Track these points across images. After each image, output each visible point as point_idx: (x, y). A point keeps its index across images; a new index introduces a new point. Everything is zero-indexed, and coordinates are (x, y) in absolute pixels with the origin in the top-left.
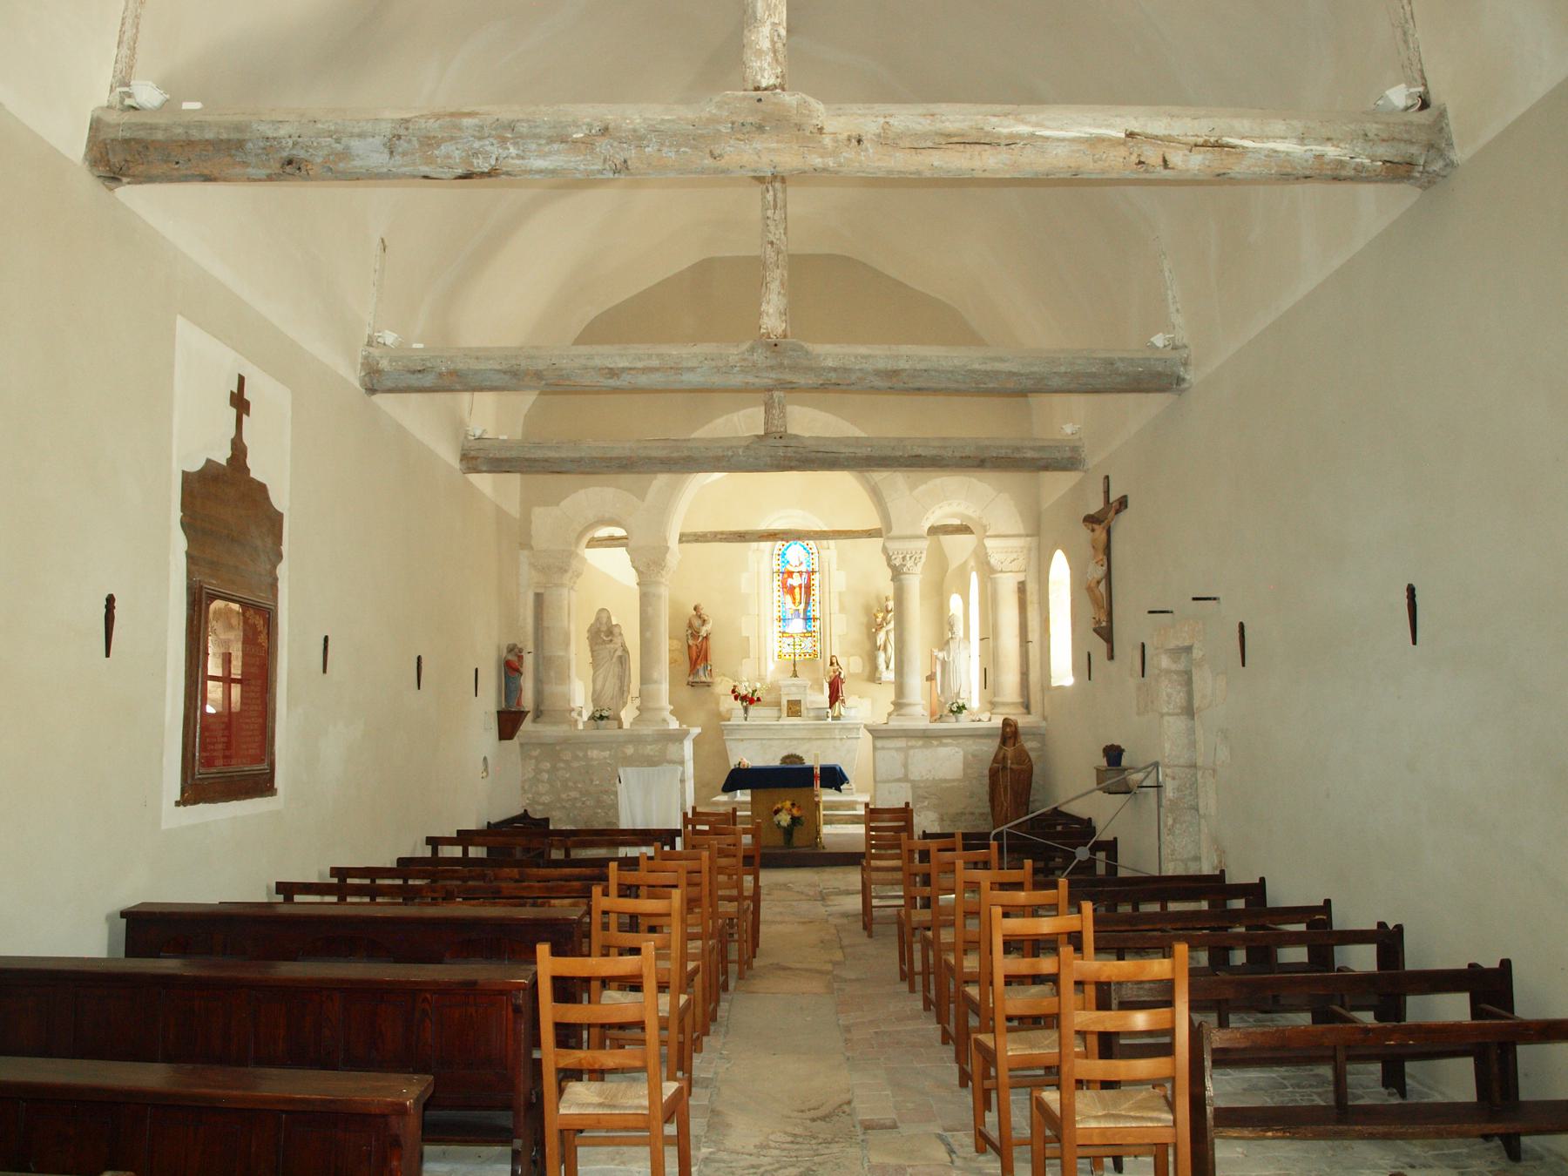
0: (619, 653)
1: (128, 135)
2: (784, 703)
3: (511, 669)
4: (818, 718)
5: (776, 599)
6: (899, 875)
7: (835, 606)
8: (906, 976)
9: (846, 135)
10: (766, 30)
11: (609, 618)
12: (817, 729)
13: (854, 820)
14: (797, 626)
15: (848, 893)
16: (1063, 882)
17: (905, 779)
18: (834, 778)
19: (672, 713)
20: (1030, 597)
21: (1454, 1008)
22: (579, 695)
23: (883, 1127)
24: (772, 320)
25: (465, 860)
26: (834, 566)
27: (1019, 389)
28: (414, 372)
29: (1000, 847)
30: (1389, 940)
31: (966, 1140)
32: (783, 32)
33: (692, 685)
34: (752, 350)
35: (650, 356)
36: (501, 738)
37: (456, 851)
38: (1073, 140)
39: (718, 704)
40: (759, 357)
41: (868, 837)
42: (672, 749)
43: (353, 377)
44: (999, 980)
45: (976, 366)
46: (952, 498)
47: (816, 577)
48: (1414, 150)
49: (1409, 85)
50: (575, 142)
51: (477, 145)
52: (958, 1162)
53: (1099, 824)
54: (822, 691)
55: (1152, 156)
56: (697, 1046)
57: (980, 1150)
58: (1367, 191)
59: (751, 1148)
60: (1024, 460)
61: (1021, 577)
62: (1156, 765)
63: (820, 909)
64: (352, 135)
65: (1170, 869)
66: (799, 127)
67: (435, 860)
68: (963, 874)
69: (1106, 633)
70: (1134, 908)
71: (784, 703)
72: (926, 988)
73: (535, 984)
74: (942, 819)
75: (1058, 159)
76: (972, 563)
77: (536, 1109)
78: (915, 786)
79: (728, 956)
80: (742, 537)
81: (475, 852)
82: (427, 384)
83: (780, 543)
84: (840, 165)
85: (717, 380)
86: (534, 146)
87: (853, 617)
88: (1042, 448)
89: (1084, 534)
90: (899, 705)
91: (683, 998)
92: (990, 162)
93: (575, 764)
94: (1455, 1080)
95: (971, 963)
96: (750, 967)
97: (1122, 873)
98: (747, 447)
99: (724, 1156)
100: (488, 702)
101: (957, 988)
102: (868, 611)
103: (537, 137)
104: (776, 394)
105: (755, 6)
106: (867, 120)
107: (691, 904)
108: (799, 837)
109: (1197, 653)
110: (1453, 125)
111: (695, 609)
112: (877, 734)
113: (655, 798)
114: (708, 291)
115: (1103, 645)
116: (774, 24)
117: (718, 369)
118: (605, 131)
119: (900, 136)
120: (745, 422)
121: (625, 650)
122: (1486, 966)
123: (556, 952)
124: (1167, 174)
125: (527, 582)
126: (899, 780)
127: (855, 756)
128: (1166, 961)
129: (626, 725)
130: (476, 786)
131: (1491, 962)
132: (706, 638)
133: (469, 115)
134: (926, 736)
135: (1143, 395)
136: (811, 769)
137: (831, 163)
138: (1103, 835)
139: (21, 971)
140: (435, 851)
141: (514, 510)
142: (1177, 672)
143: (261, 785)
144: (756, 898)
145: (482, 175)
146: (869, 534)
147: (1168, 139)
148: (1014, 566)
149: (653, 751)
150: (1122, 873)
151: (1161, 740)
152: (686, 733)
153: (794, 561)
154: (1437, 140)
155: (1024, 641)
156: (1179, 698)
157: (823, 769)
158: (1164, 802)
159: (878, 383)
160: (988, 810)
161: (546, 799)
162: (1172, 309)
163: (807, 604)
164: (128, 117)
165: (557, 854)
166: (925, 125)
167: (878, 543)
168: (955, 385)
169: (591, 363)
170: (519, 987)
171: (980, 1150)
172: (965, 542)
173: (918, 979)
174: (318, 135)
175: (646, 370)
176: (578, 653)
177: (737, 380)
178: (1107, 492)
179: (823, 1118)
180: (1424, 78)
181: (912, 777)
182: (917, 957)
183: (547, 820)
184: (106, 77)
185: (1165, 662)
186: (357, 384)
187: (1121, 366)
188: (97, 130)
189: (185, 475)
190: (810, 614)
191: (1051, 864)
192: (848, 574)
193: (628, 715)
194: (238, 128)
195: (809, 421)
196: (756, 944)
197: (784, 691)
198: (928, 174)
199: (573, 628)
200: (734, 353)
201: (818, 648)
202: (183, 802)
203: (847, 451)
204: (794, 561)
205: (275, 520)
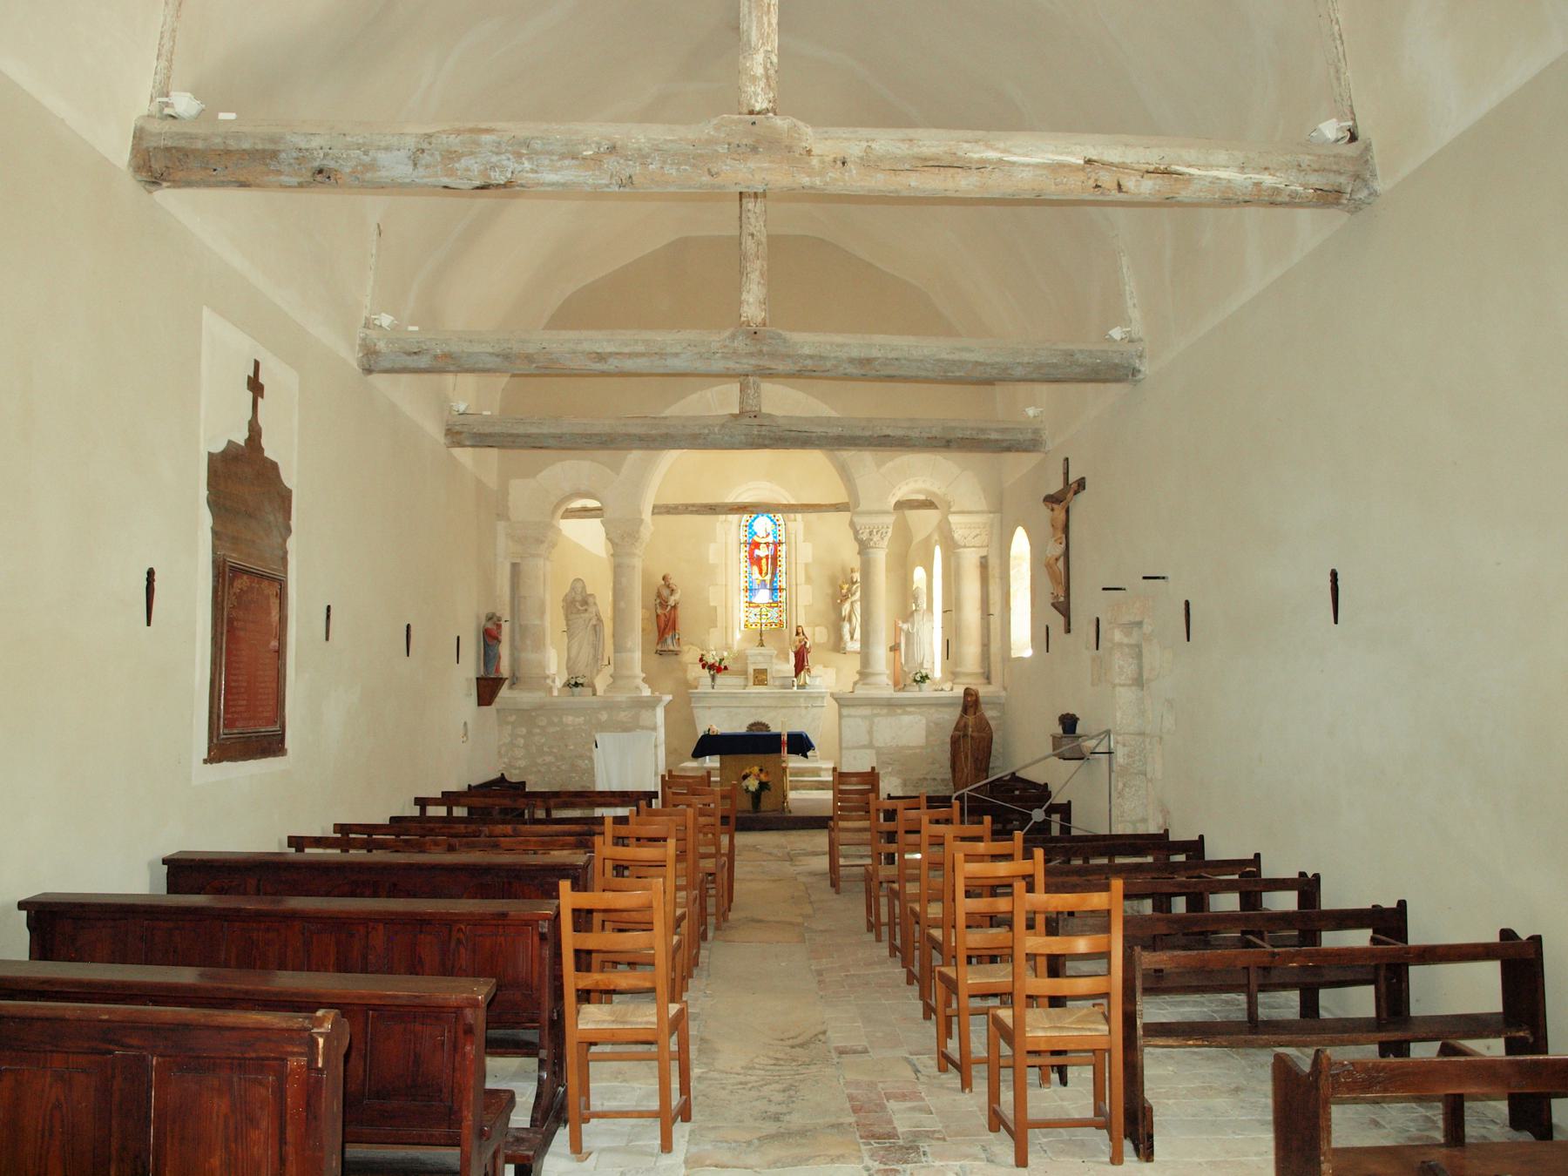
0: (594, 622)
1: (169, 143)
2: (751, 671)
3: (490, 637)
4: (783, 687)
5: (743, 569)
6: (867, 836)
7: (802, 578)
8: (873, 926)
9: (831, 158)
10: (760, 57)
11: (584, 587)
13: (821, 786)
14: (763, 596)
15: (815, 854)
16: (1019, 835)
17: (870, 746)
18: (800, 744)
19: (644, 680)
20: (993, 572)
21: (1360, 938)
22: (554, 663)
23: (855, 1052)
24: (753, 305)
25: (449, 819)
26: (801, 537)
27: (987, 379)
28: (409, 354)
29: (962, 809)
30: (1308, 887)
31: (929, 1062)
32: (775, 60)
33: (660, 653)
34: (733, 337)
35: (636, 341)
36: (480, 704)
37: (441, 811)
38: (1037, 166)
39: (685, 671)
40: (740, 344)
41: (835, 800)
42: (645, 715)
43: (352, 358)
44: (961, 921)
45: (944, 356)
46: (918, 474)
47: (783, 548)
48: (1342, 179)
49: (1341, 118)
50: (584, 158)
51: (494, 159)
52: (922, 1079)
53: (1053, 788)
55: (1107, 179)
56: (684, 988)
57: (942, 1069)
58: (1304, 215)
59: (738, 1069)
60: (988, 441)
61: (983, 552)
62: (1108, 733)
63: (788, 868)
64: (379, 149)
65: (1119, 829)
66: (790, 149)
67: (423, 818)
68: (929, 829)
69: (1064, 608)
70: (1077, 855)
71: (751, 671)
72: (892, 936)
73: (558, 915)
74: (905, 784)
75: (1024, 182)
76: (936, 537)
77: (557, 1028)
79: (711, 906)
80: (713, 509)
81: (460, 812)
82: (422, 366)
83: (746, 517)
84: (826, 184)
85: (700, 366)
86: (547, 162)
87: (832, 591)
88: (1004, 431)
89: (1044, 512)
90: (864, 674)
91: (676, 938)
92: (965, 183)
93: (551, 730)
94: (1360, 1001)
95: (935, 910)
96: (726, 919)
97: (1074, 832)
98: (723, 426)
99: (715, 1075)
100: (469, 668)
101: (922, 932)
102: (833, 581)
103: (551, 153)
104: (751, 379)
105: (749, 35)
106: (852, 143)
107: (681, 856)
108: (767, 803)
109: (1147, 628)
110: (1377, 158)
111: (664, 578)
112: (842, 702)
113: (632, 761)
114: (685, 276)
115: (1061, 619)
116: (767, 51)
117: (701, 356)
118: (612, 149)
119: (881, 159)
120: (720, 400)
121: (599, 620)
122: (1385, 905)
123: (576, 887)
124: (1121, 197)
125: (504, 550)
126: (864, 747)
127: (818, 723)
128: (1104, 894)
129: (599, 693)
130: (458, 751)
131: (1390, 903)
132: (674, 607)
133: (487, 131)
134: (891, 705)
135: (1101, 386)
136: (779, 736)
137: (818, 182)
138: (1058, 798)
139: (101, 905)
140: (423, 810)
141: (492, 481)
142: (1129, 646)
143: (272, 745)
144: (731, 856)
145: (498, 186)
146: (837, 508)
147: (1122, 166)
148: (977, 542)
149: (629, 718)
150: (1074, 832)
151: (1116, 711)
152: (659, 700)
154: (1362, 172)
155: (986, 613)
156: (1131, 670)
157: (790, 736)
158: (1115, 767)
159: (851, 370)
160: (949, 776)
161: (522, 763)
162: (1130, 303)
163: (774, 574)
164: (167, 126)
165: (541, 814)
166: (903, 149)
167: (845, 516)
168: (923, 374)
169: (580, 348)
170: (545, 917)
171: (942, 1069)
172: (930, 517)
173: (885, 929)
174: (348, 148)
175: (630, 355)
176: (552, 621)
177: (718, 365)
178: (1066, 474)
179: (801, 1045)
180: (1352, 113)
181: (877, 744)
182: (884, 910)
183: (523, 784)
184: (147, 86)
185: (1118, 636)
186: (355, 365)
187: (1080, 358)
188: (141, 138)
189: (210, 455)
191: (1009, 827)
192: (812, 547)
193: (601, 683)
194: (273, 140)
195: (782, 401)
196: (730, 900)
197: (751, 660)
198: (905, 193)
199: (548, 597)
200: (717, 339)
201: (784, 618)
202: (210, 760)
203: (819, 430)
205: (284, 498)
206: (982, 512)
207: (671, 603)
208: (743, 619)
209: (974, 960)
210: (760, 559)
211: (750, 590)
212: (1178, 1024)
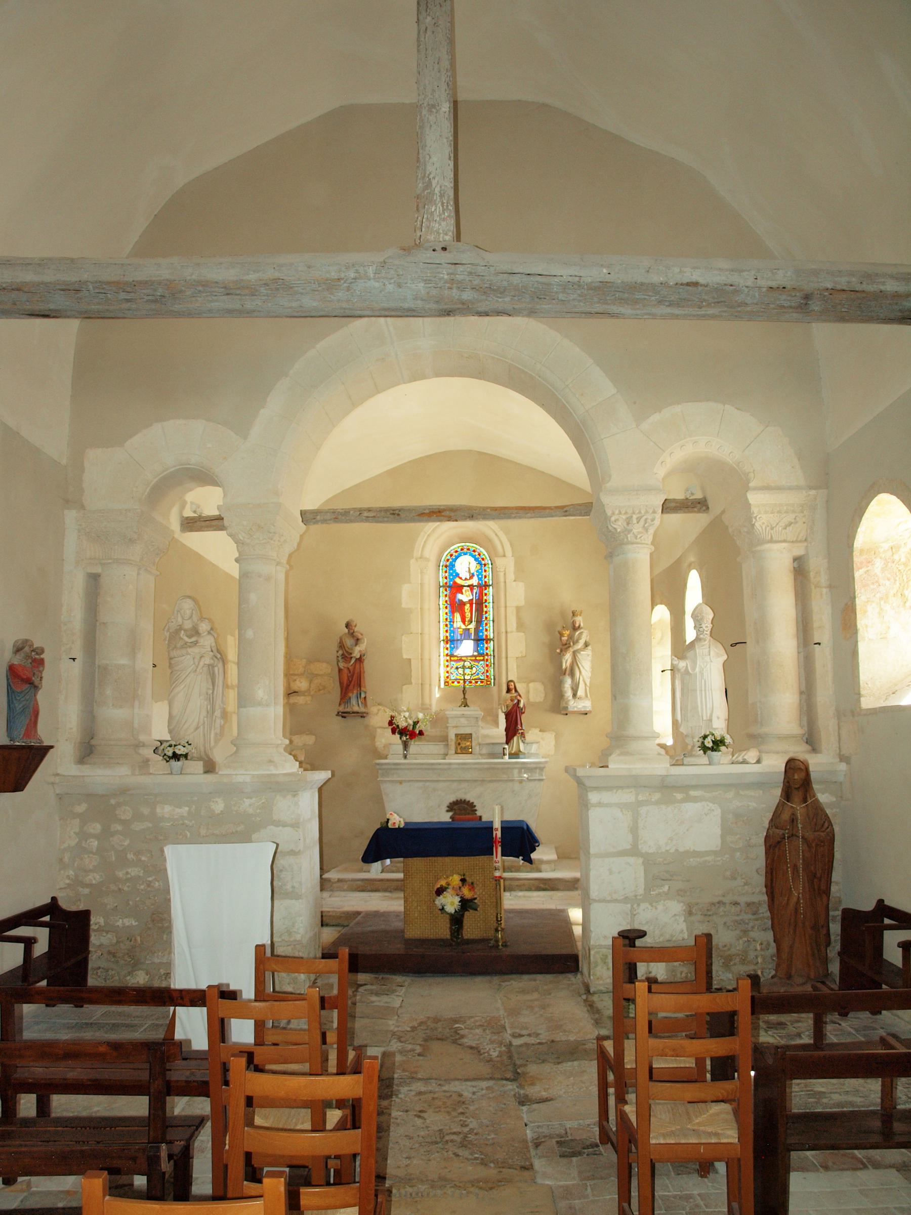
4: (493, 755)
5: (443, 617)
12: (491, 768)
14: (467, 648)
17: (634, 851)
26: (511, 576)
33: (343, 715)
39: (373, 737)
54: (496, 724)
61: (799, 551)
76: (692, 558)
78: (648, 861)
93: (138, 826)
102: (549, 627)
108: (472, 928)
111: (348, 625)
153: (464, 574)
161: (95, 878)
163: (479, 622)
181: (644, 848)
190: (483, 634)
197: (451, 723)
204: (464, 574)
206: (798, 488)
207: (356, 654)
208: (443, 675)
209: (355, 706)
210: (462, 604)
211: (452, 641)
212: (215, 530)
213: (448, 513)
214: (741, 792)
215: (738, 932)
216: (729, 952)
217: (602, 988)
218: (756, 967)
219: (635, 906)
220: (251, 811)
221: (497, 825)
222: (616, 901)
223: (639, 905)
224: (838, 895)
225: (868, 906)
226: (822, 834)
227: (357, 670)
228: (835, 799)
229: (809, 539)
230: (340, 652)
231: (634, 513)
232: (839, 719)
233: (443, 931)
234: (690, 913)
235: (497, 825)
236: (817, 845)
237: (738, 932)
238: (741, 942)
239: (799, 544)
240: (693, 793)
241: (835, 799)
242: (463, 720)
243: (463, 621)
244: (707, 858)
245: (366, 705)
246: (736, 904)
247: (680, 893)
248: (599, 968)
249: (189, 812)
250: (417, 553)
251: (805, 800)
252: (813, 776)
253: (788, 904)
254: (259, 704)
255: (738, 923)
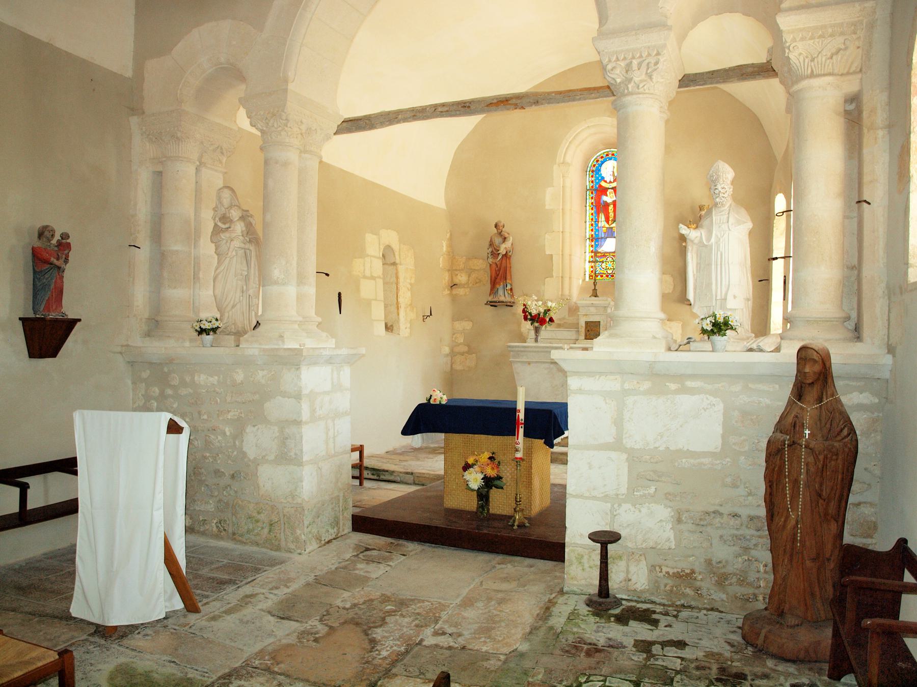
2: (582, 323)
17: (617, 445)
33: (493, 304)
61: (851, 86)
78: (634, 458)
108: (500, 503)
111: (496, 226)
132: (506, 256)
153: (609, 178)
155: (856, 200)
160: (762, 512)
181: (628, 443)
197: (582, 311)
204: (609, 178)
207: (502, 251)
209: (502, 296)
210: (607, 205)
213: (514, 101)
214: (750, 385)
215: (737, 548)
216: (723, 570)
217: (575, 589)
218: (756, 591)
219: (616, 506)
220: (263, 382)
221: (521, 407)
222: (594, 498)
223: (620, 505)
224: (873, 519)
225: (883, 543)
226: (836, 444)
227: (504, 265)
228: (877, 401)
229: (864, 70)
230: (490, 250)
231: (633, 58)
232: (889, 298)
233: (471, 504)
234: (679, 521)
235: (521, 407)
236: (826, 457)
237: (737, 548)
238: (740, 559)
239: (850, 77)
240: (689, 384)
241: (877, 401)
242: (593, 310)
243: (607, 220)
244: (703, 460)
245: (512, 296)
246: (735, 515)
247: (669, 496)
248: (574, 567)
249: (219, 381)
250: (559, 159)
251: (820, 400)
252: (836, 369)
253: (784, 526)
254: (276, 283)
255: (739, 538)
